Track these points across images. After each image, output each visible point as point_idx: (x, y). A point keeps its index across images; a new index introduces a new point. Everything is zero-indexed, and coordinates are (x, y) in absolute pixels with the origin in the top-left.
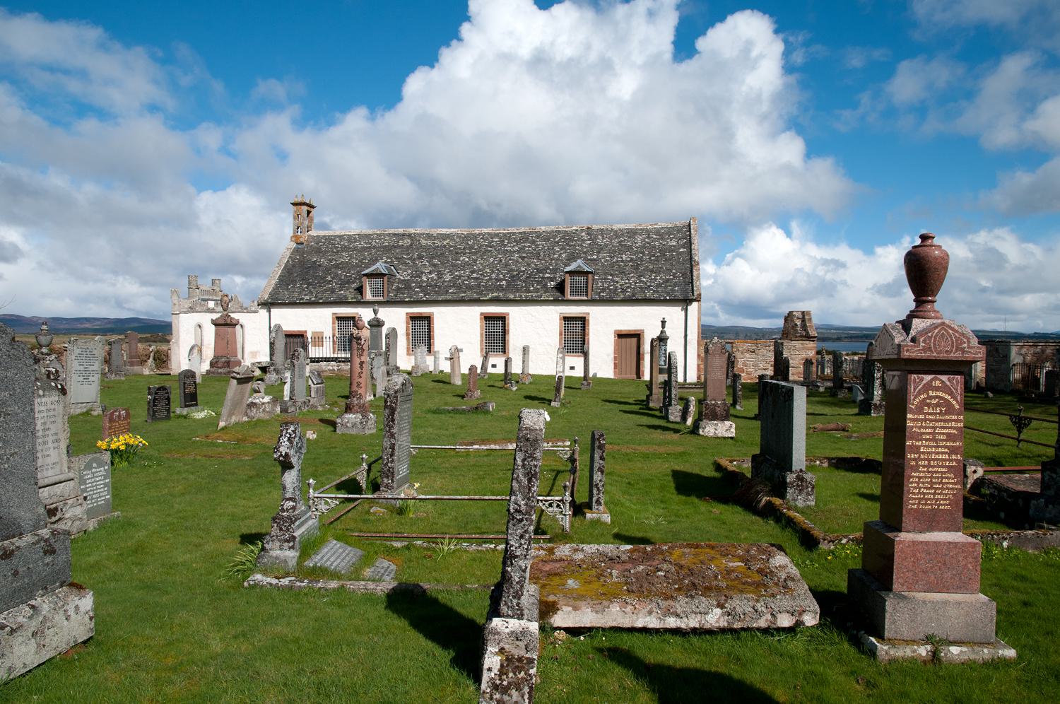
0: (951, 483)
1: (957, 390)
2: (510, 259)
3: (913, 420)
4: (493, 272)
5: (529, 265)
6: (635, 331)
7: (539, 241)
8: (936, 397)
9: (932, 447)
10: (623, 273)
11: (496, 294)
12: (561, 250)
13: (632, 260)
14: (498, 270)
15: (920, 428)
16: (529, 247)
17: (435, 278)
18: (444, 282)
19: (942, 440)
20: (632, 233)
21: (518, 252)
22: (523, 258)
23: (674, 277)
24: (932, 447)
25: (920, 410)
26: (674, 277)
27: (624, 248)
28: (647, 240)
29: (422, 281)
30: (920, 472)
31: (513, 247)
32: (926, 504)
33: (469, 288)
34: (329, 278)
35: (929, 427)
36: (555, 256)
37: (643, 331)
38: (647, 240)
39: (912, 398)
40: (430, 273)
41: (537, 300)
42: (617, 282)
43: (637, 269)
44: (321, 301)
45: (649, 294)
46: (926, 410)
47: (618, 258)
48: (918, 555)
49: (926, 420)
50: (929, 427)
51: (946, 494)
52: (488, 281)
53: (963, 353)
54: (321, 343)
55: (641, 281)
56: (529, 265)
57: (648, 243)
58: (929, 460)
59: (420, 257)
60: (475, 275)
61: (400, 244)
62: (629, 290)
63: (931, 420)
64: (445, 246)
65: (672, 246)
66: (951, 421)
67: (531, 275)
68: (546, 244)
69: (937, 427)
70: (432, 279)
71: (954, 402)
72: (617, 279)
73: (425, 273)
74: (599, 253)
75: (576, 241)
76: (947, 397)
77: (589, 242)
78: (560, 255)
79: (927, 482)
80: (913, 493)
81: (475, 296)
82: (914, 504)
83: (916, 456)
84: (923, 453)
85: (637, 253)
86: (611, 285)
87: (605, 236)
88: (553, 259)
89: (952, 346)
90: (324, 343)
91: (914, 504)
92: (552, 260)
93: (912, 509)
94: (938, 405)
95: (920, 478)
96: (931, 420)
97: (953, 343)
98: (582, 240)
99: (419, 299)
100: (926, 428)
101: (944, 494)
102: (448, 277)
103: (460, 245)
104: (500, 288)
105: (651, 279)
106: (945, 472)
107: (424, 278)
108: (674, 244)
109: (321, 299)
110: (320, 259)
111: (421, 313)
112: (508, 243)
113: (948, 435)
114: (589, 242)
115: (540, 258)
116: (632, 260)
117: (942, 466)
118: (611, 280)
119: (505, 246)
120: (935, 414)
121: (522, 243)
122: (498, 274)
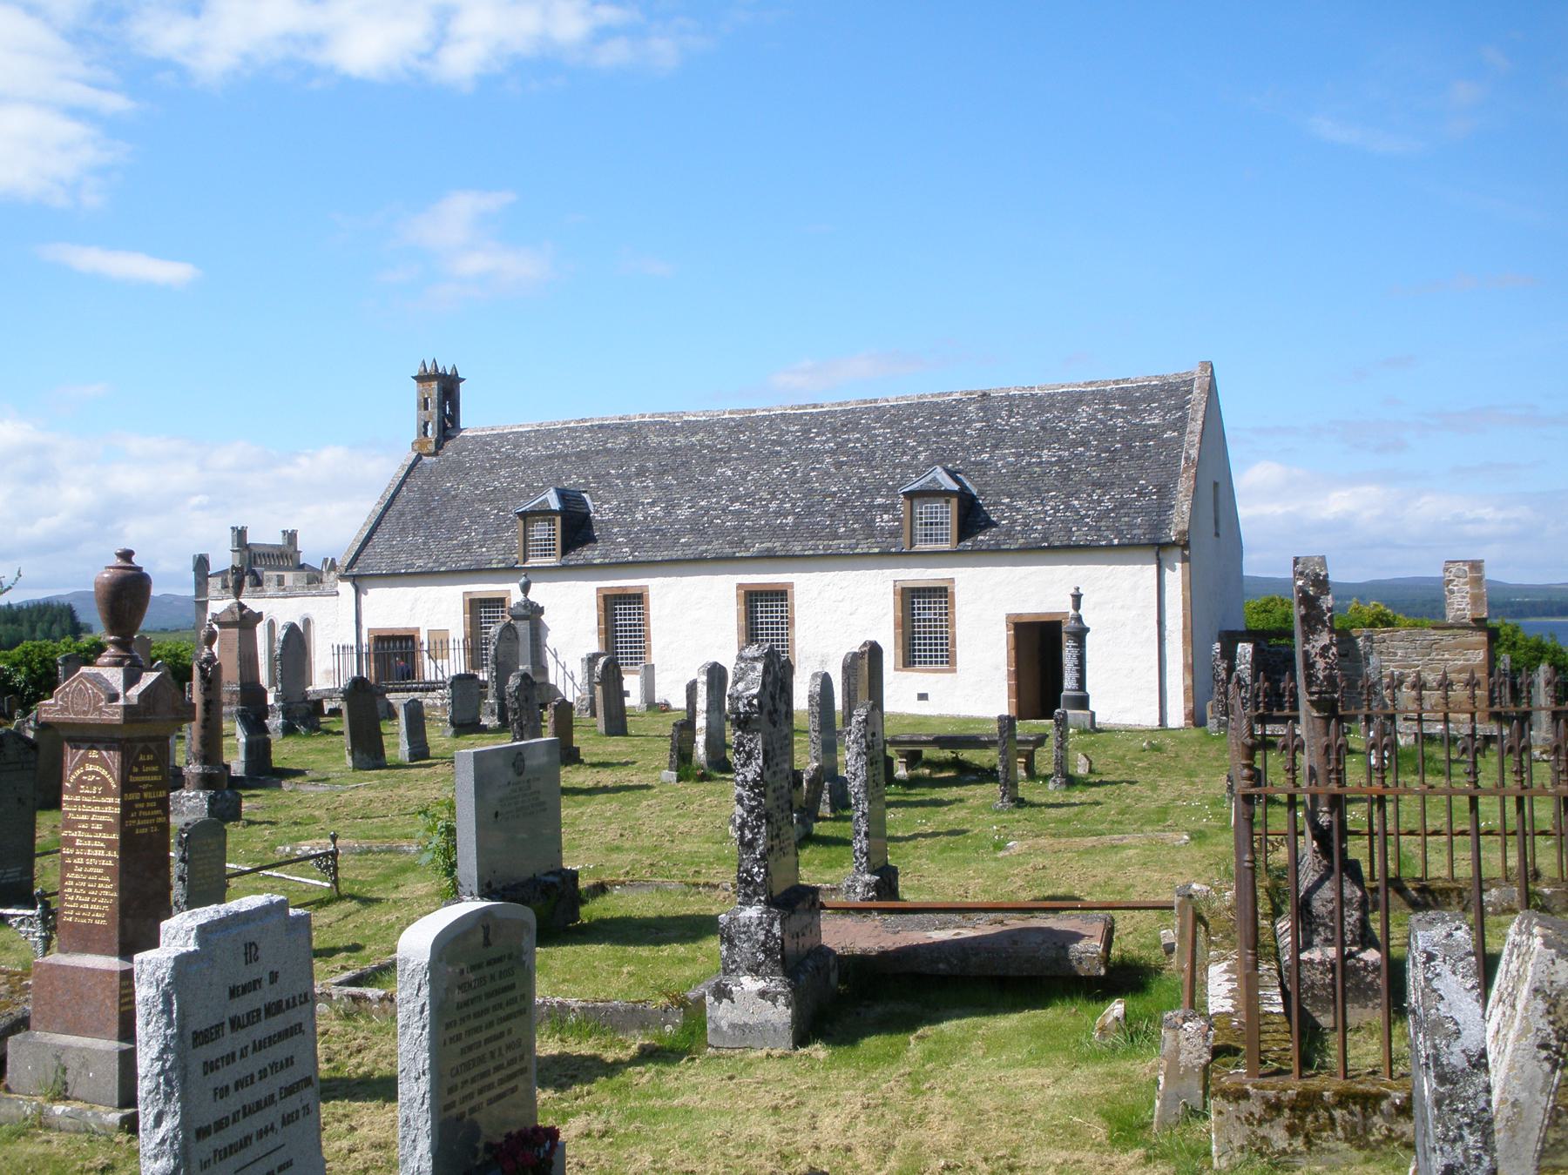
0: (107, 890)
1: (113, 763)
2: (813, 469)
3: (71, 803)
4: (774, 497)
5: (847, 479)
6: (1051, 614)
7: (881, 428)
8: (93, 773)
9: (87, 839)
10: (1036, 492)
11: (770, 545)
12: (919, 444)
13: (1060, 460)
14: (785, 493)
15: (76, 813)
16: (858, 440)
17: (660, 514)
18: (677, 521)
19: (99, 831)
20: (1074, 400)
21: (833, 452)
22: (839, 465)
23: (1140, 494)
24: (87, 839)
25: (75, 791)
26: (1140, 494)
27: (1055, 435)
28: (1100, 416)
29: (634, 522)
30: (76, 873)
31: (825, 442)
32: (81, 917)
33: (721, 532)
34: (466, 522)
35: (85, 813)
36: (905, 459)
37: (1008, 616)
38: (1100, 416)
39: (69, 773)
40: (652, 504)
41: (845, 555)
42: (1018, 510)
43: (1067, 478)
44: (443, 569)
45: (1078, 536)
46: (83, 789)
47: (1032, 456)
48: (56, 983)
49: (81, 803)
50: (85, 813)
51: (102, 904)
52: (759, 517)
53: (100, 714)
54: (444, 652)
55: (1068, 507)
56: (847, 479)
57: (1100, 421)
58: (85, 857)
59: (641, 472)
60: (737, 506)
61: (609, 445)
62: (1039, 527)
63: (87, 804)
64: (693, 445)
65: (1150, 426)
66: (107, 805)
67: (846, 501)
68: (891, 433)
69: (94, 813)
70: (654, 518)
71: (111, 780)
72: (1019, 504)
73: (643, 504)
74: (996, 446)
75: (953, 424)
76: (104, 772)
77: (978, 425)
78: (914, 457)
79: (82, 887)
80: (69, 901)
81: (728, 550)
82: (68, 916)
83: (72, 851)
84: (79, 847)
85: (1074, 444)
86: (1005, 518)
87: (1015, 410)
88: (900, 465)
89: (90, 706)
90: (451, 652)
91: (68, 916)
92: (896, 466)
93: (67, 922)
94: (94, 783)
95: (75, 880)
96: (87, 804)
97: (90, 700)
98: (967, 422)
99: (620, 560)
100: (82, 813)
101: (100, 904)
102: (684, 512)
103: (722, 443)
104: (776, 532)
105: (1093, 501)
106: (100, 875)
107: (639, 516)
108: (1156, 421)
109: (443, 564)
110: (458, 484)
111: (625, 588)
112: (818, 434)
113: (104, 823)
114: (978, 425)
115: (873, 463)
116: (1060, 460)
117: (98, 866)
118: (1008, 506)
119: (811, 440)
120: (91, 795)
121: (845, 433)
122: (783, 502)
